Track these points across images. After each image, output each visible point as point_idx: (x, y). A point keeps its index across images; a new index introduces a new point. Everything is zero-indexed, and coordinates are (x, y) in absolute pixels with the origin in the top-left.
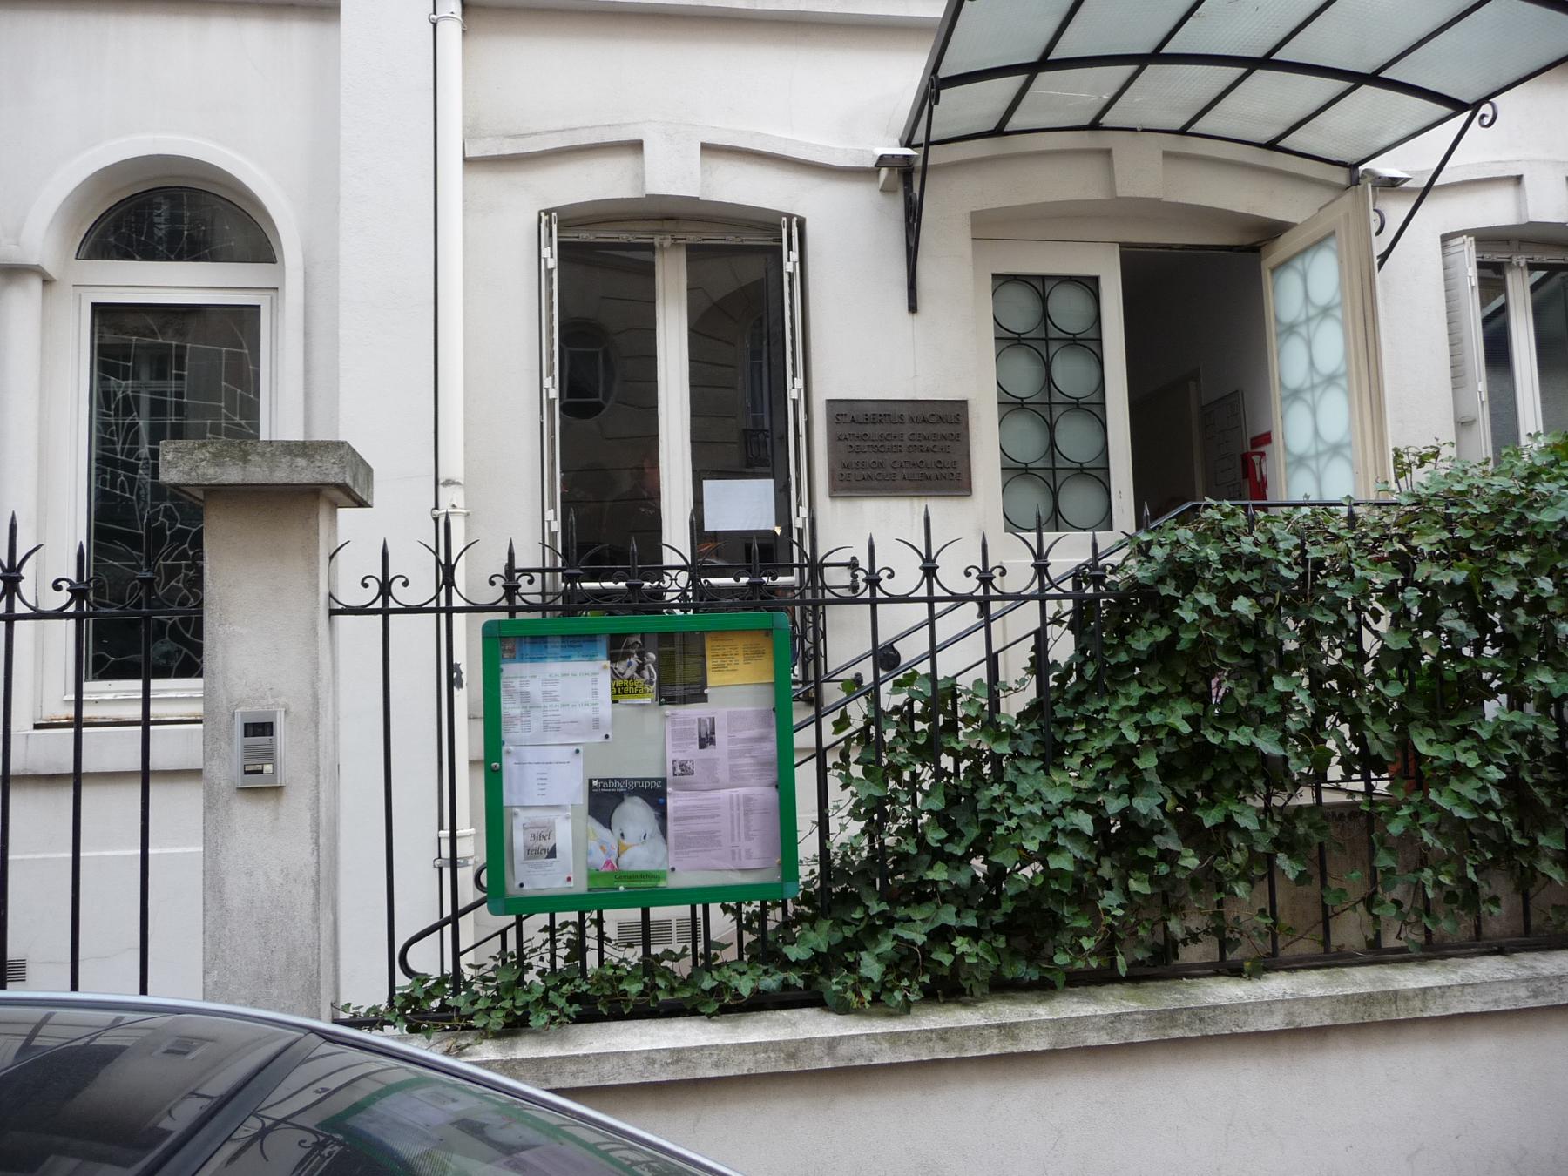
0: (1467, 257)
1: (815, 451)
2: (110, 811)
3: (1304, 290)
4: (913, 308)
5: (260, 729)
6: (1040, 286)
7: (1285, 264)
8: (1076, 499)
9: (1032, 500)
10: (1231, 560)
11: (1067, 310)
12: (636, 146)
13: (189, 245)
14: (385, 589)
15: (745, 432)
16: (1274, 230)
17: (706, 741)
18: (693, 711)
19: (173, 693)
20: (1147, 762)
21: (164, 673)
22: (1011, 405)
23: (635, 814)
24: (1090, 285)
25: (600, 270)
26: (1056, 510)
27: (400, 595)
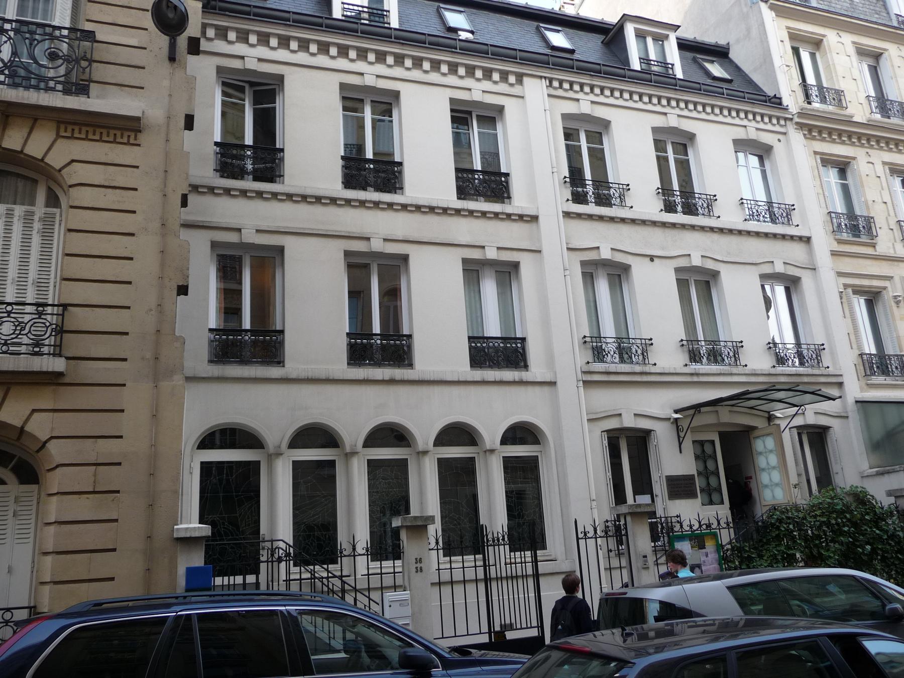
0: (795, 431)
1: (659, 487)
3: (764, 445)
5: (645, 557)
7: (758, 437)
10: (789, 518)
11: (708, 449)
12: (620, 415)
13: (522, 442)
15: (643, 484)
16: (754, 428)
17: (707, 556)
18: (704, 551)
19: (398, 563)
20: (779, 557)
23: (697, 569)
24: (713, 442)
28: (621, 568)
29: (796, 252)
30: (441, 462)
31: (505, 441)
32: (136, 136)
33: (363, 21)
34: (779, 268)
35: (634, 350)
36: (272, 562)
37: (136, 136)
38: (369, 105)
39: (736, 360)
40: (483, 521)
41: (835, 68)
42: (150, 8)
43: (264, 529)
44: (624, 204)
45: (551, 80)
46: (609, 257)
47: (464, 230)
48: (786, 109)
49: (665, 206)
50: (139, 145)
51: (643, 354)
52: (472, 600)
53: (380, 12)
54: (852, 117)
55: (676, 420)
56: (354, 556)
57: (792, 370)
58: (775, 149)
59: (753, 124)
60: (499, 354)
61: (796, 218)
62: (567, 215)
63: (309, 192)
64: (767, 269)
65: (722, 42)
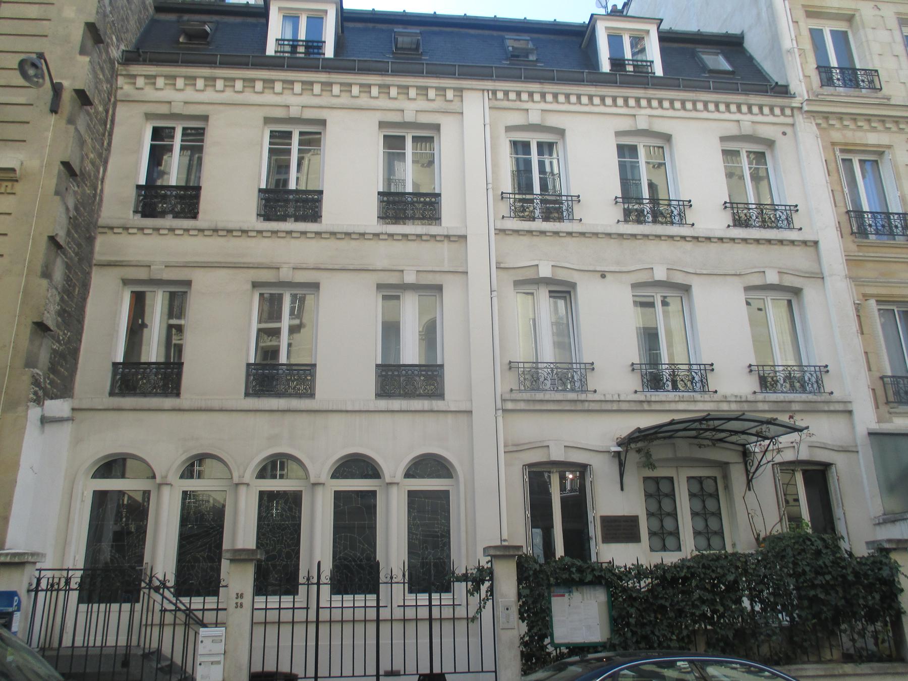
2: (286, 630)
4: (622, 489)
6: (657, 480)
8: (670, 541)
9: (657, 541)
14: (391, 578)
21: (209, 595)
22: (650, 515)
25: (537, 480)
26: (664, 545)
27: (394, 580)
28: (307, 622)
29: (799, 259)
30: (338, 494)
31: (408, 475)
32: (13, 186)
33: (298, 55)
34: (772, 278)
35: (806, 378)
36: (52, 591)
37: (13, 186)
38: (295, 140)
39: (819, 388)
40: (379, 557)
41: (868, 46)
42: (16, 67)
43: (147, 559)
44: (571, 217)
45: (494, 92)
46: (549, 275)
47: (383, 255)
48: (793, 96)
49: (734, 220)
50: (14, 194)
51: (817, 382)
52: (299, 643)
53: (315, 44)
54: (889, 99)
55: (618, 453)
56: (392, 583)
57: (780, 397)
58: (777, 144)
59: (749, 117)
60: (406, 381)
61: (797, 221)
62: (501, 232)
63: (220, 225)
64: (756, 281)
65: (734, 30)
